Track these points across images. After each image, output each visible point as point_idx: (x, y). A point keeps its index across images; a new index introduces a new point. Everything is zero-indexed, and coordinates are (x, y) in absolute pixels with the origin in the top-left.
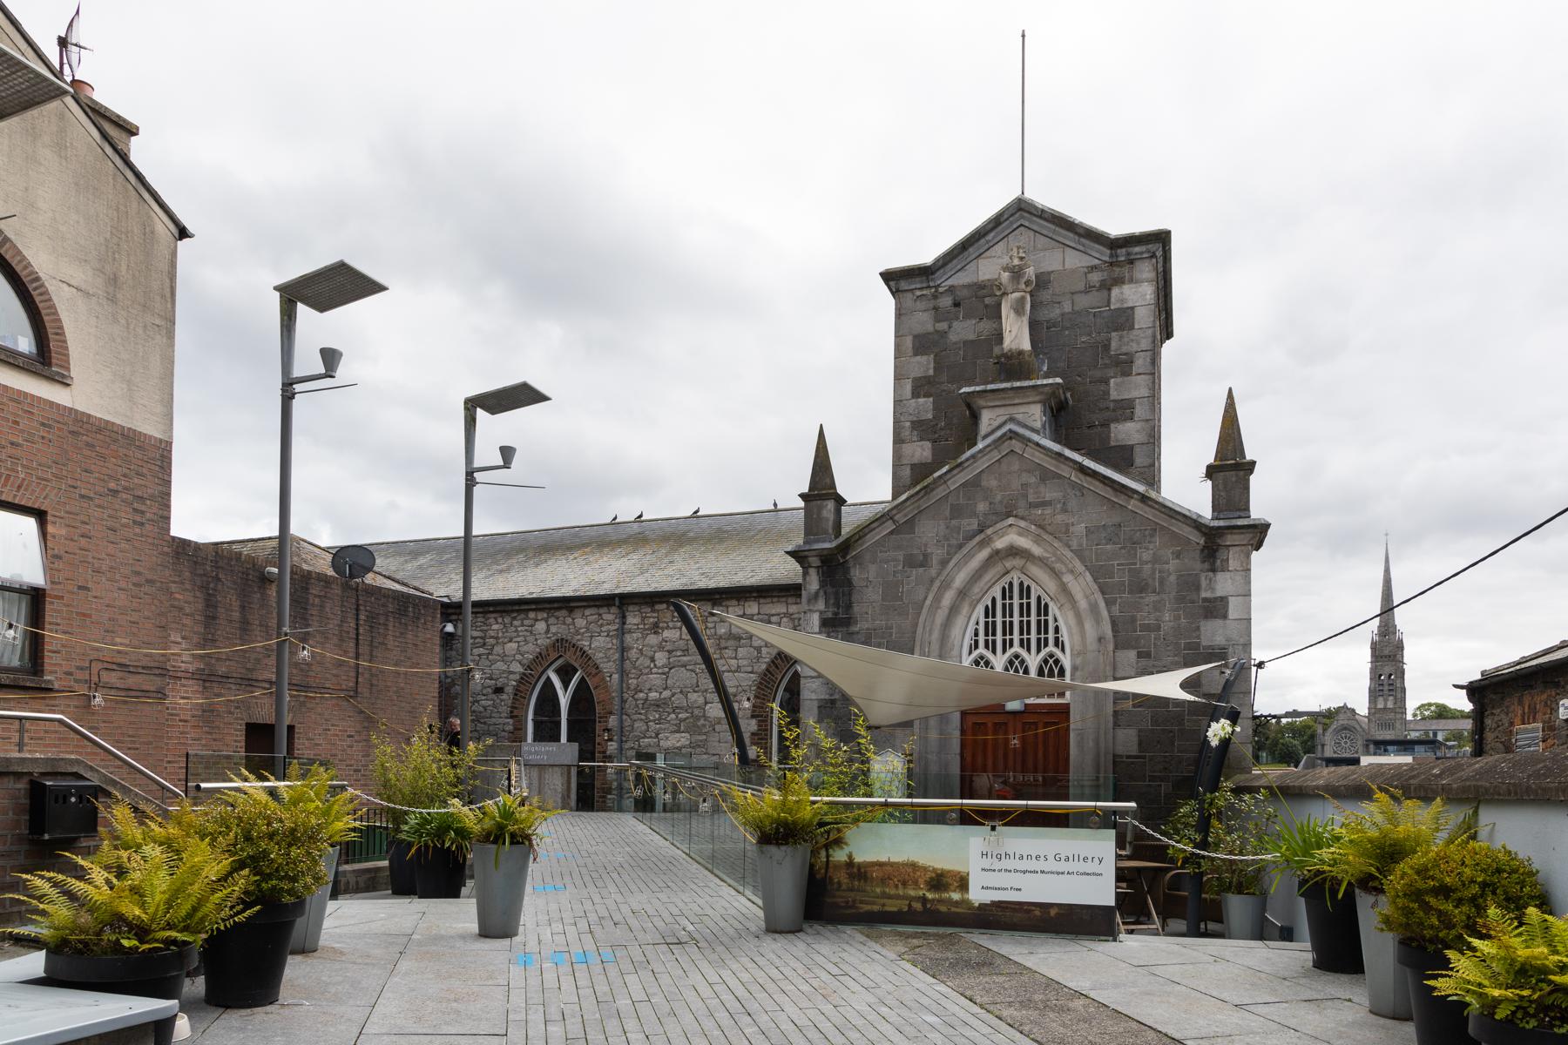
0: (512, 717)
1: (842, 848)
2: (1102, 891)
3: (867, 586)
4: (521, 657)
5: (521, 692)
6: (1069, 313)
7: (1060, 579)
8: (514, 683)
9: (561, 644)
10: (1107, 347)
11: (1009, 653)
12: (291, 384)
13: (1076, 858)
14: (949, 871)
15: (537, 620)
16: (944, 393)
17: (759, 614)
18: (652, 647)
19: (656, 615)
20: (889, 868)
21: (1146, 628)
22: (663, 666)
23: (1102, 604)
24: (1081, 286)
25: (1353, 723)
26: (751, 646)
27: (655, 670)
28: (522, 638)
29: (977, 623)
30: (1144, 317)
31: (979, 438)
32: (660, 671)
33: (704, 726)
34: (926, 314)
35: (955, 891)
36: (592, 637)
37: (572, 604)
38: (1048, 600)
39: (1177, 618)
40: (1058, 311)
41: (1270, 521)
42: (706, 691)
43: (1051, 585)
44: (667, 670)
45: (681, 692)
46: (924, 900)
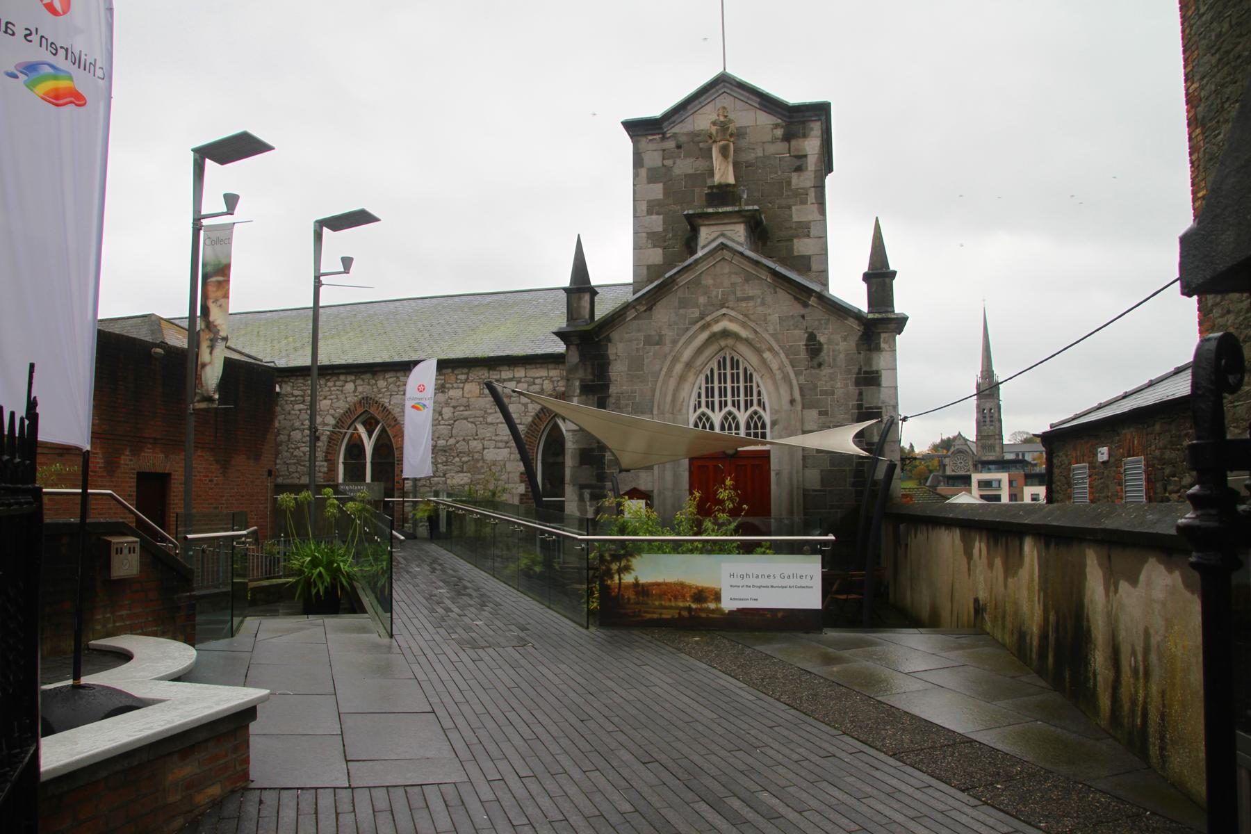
0: (326, 461)
1: (630, 573)
2: (812, 599)
3: (616, 360)
4: (334, 412)
5: (334, 440)
6: (760, 157)
7: (762, 356)
8: (328, 433)
9: (366, 400)
10: (789, 183)
11: (725, 410)
12: (200, 219)
13: (795, 575)
14: (707, 588)
15: (346, 382)
16: (671, 212)
17: (526, 377)
18: (440, 404)
19: (443, 377)
20: (664, 587)
21: (824, 393)
22: (449, 419)
23: (792, 375)
24: (769, 138)
25: (965, 448)
26: (519, 403)
27: (442, 422)
28: (335, 396)
29: (700, 388)
30: (812, 162)
31: (699, 248)
32: (447, 423)
33: (482, 467)
34: (655, 153)
35: (711, 602)
36: (391, 395)
37: (375, 369)
38: (752, 370)
39: (846, 385)
40: (753, 155)
41: (908, 315)
42: (484, 439)
43: (753, 359)
44: (452, 422)
45: (464, 440)
46: (689, 609)
